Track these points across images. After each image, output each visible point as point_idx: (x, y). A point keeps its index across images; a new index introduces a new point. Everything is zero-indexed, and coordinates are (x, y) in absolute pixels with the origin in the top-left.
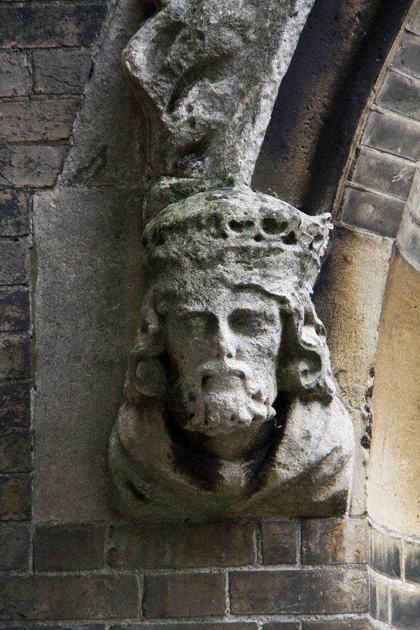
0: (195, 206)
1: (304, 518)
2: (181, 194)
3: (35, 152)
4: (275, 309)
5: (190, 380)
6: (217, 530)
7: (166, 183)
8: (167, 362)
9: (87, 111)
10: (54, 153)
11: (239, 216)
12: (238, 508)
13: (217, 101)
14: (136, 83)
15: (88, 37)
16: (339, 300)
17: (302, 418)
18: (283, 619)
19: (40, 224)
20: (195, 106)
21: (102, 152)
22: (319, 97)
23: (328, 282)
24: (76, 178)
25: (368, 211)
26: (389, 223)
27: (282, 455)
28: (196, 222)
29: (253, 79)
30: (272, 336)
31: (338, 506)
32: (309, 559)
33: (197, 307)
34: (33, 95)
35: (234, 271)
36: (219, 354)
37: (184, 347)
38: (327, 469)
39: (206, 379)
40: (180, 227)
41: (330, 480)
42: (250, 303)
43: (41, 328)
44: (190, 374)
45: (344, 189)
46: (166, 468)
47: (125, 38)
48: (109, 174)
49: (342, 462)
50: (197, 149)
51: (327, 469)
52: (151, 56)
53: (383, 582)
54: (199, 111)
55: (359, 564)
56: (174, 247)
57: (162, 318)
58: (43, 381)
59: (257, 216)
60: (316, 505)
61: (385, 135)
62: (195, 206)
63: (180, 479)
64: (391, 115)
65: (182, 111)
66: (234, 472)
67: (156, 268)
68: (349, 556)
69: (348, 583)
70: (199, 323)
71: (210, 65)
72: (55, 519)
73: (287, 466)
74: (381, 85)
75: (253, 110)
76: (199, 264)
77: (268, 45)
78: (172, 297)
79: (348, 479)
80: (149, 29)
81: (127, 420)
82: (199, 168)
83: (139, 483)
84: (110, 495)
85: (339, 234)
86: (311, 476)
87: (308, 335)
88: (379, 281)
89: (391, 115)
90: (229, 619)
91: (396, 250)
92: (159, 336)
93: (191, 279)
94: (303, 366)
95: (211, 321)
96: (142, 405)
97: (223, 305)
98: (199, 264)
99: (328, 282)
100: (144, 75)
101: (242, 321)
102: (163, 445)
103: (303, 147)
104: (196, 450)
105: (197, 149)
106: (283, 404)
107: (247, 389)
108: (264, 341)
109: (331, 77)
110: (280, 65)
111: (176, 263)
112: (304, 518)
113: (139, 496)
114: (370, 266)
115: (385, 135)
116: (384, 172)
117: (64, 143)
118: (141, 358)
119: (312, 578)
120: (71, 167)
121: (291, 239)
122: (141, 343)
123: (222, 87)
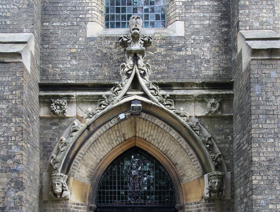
0: (54, 174)
1: (66, 200)
2: (54, 173)
3: (43, 169)
4: (61, 183)
5: (54, 189)
6: (58, 201)
7: (53, 172)
8: (52, 187)
9: (48, 166)
10: (45, 169)
11: (58, 175)
12: (60, 199)
13: (58, 165)
14: (51, 164)
15: (48, 160)
16: (68, 183)
17: (64, 192)
18: (162, 124)
19: (43, 175)
20: (56, 166)
21: (49, 169)
22: (67, 165)
23: (67, 181)
24: (46, 172)
25: (71, 175)
26: (73, 176)
27: (63, 195)
28: (54, 176)
29: (60, 164)
30: (61, 185)
31: (68, 199)
32: (66, 204)
33: (54, 183)
34: (43, 165)
35: (57, 180)
36: (56, 187)
37: (54, 186)
38: (67, 196)
39: (55, 189)
40: (53, 176)
41: (67, 197)
42: (58, 182)
43: (43, 184)
44: (211, 131)
45: (69, 173)
46: (53, 196)
47: (51, 160)
48: (49, 171)
49: (68, 196)
50: (56, 169)
51: (67, 196)
52: (53, 161)
53: (73, 205)
54: (56, 166)
55: (70, 204)
56: (52, 178)
57: (52, 184)
58: (43, 188)
59: (59, 175)
60: (66, 199)
61: (73, 168)
62: (54, 174)
63: (54, 197)
64: (73, 167)
65: (55, 166)
66: (59, 196)
67: (51, 179)
68: (69, 203)
69: (69, 205)
70: (54, 184)
71: (57, 162)
72: (45, 200)
73: (63, 196)
74: (73, 164)
75: (60, 166)
76: (54, 179)
77: (62, 161)
78: (52, 182)
79: (69, 197)
80: (52, 159)
81: (50, 192)
82: (56, 171)
83: (51, 197)
84: (49, 199)
85: (69, 177)
86: (65, 197)
87: (64, 185)
88: (72, 181)
89: (73, 167)
90: (59, 208)
91: (74, 178)
92: (51, 185)
93: (54, 180)
94: (64, 188)
95: (55, 184)
96: (51, 191)
97: (56, 183)
98: (54, 179)
99: (67, 181)
100: (52, 163)
101: (58, 184)
102: (53, 194)
103: (66, 169)
104: (55, 195)
105: (56, 169)
106: (63, 191)
107: (59, 189)
108: (60, 186)
109: (68, 163)
110: (63, 162)
111: (52, 179)
112: (66, 200)
113: (51, 198)
114: (71, 179)
115: (73, 168)
116: (73, 172)
117: (46, 169)
118: (50, 187)
119: (66, 205)
120: (46, 171)
121: (62, 177)
122: (50, 186)
123: (58, 164)
